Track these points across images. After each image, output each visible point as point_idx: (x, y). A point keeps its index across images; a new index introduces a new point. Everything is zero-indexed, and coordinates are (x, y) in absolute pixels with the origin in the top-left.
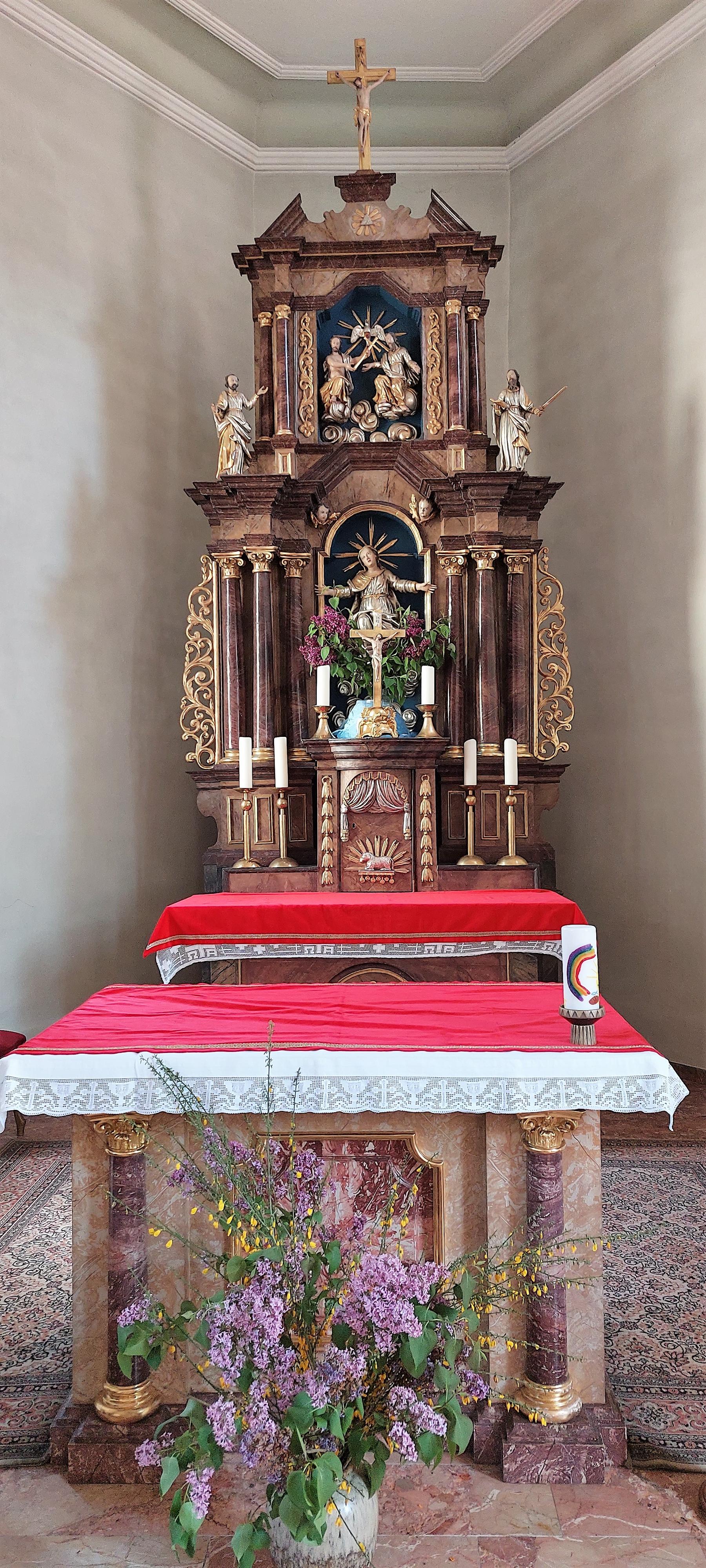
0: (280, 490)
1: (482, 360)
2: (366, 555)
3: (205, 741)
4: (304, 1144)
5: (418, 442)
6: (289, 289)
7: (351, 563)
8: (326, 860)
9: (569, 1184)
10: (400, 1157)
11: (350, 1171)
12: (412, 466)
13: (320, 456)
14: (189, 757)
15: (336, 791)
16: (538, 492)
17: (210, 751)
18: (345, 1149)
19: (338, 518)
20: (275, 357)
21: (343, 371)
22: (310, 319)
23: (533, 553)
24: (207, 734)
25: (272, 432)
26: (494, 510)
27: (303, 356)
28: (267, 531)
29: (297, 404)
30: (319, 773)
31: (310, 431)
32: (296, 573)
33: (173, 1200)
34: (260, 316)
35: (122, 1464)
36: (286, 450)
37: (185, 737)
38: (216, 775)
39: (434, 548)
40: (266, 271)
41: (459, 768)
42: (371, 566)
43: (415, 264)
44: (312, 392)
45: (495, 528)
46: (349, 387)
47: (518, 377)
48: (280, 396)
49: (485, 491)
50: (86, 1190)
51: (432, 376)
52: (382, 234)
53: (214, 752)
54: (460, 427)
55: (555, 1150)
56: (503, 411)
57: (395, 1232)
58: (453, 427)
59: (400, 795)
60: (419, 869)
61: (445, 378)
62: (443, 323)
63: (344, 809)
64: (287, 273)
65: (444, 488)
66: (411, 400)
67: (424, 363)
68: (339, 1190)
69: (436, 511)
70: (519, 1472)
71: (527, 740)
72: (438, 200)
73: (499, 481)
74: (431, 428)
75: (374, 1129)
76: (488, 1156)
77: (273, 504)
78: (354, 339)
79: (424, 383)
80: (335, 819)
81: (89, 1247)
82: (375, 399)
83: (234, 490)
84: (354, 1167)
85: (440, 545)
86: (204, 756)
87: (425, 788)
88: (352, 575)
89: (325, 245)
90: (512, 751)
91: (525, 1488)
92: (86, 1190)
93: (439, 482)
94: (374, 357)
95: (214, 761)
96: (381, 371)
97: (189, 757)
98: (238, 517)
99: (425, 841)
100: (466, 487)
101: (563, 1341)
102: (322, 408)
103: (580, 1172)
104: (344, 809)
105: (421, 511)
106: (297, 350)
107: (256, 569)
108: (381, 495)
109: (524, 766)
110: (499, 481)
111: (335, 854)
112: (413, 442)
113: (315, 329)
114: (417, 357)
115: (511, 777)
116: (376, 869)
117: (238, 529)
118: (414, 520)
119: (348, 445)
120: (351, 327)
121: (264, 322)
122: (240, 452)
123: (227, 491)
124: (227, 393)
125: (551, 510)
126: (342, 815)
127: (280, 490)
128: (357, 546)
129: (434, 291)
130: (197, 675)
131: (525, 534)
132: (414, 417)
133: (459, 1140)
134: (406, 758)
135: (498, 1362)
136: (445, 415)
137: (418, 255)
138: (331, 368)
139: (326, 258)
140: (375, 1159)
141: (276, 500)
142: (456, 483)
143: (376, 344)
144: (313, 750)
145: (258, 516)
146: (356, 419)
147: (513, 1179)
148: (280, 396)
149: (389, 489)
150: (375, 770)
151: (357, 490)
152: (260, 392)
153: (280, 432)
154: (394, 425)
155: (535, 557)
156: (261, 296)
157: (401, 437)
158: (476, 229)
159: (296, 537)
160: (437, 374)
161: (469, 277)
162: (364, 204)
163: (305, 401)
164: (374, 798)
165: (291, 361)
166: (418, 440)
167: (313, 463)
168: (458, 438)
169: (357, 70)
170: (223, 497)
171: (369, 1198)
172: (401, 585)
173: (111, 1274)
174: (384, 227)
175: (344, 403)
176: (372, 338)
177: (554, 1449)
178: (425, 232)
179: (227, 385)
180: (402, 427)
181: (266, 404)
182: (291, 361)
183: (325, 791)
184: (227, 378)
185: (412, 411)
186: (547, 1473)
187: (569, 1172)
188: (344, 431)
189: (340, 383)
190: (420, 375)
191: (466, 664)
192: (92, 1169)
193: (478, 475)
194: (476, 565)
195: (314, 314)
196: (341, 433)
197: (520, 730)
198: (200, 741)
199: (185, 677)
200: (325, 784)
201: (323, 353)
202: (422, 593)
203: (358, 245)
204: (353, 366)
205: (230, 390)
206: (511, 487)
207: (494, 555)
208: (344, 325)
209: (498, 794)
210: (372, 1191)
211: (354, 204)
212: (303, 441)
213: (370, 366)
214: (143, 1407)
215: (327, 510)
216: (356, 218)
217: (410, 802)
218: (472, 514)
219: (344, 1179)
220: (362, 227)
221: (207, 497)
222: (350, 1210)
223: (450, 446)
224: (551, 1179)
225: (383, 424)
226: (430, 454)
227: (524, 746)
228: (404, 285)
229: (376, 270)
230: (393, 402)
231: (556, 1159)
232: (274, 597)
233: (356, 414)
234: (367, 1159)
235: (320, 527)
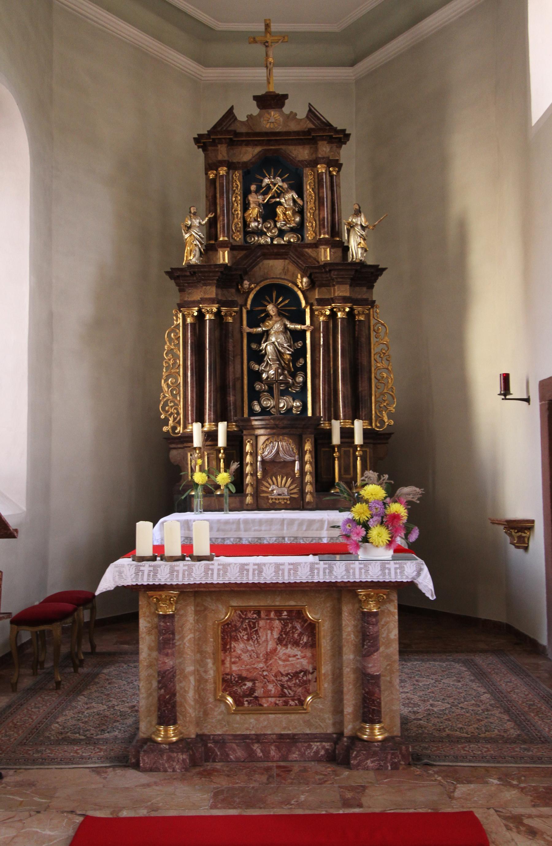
0: (221, 272)
1: (339, 197)
2: (271, 309)
3: (175, 419)
4: (252, 612)
5: (302, 244)
6: (226, 158)
7: (262, 313)
8: (249, 490)
9: (382, 628)
10: (299, 618)
11: (275, 625)
12: (298, 257)
13: (244, 252)
14: (165, 429)
15: (255, 448)
16: (372, 273)
17: (177, 425)
18: (272, 615)
19: (255, 287)
20: (218, 195)
21: (257, 203)
22: (237, 175)
23: (370, 309)
24: (176, 415)
25: (216, 238)
26: (346, 284)
27: (234, 195)
28: (213, 296)
29: (231, 222)
30: (245, 437)
31: (238, 237)
32: (230, 320)
33: (189, 637)
34: (209, 173)
35: (166, 762)
36: (224, 249)
37: (163, 417)
38: (182, 440)
39: (311, 305)
40: (213, 148)
41: (329, 434)
42: (275, 315)
43: (299, 144)
44: (239, 216)
45: (347, 294)
46: (261, 212)
47: (360, 208)
48: (221, 218)
49: (342, 273)
50: (146, 633)
51: (310, 206)
52: (280, 127)
53: (180, 426)
54: (327, 236)
55: (375, 610)
56: (351, 227)
57: (297, 655)
58: (322, 236)
59: (293, 450)
60: (304, 495)
61: (317, 208)
62: (316, 177)
63: (259, 458)
64: (225, 149)
65: (317, 271)
66: (298, 219)
67: (305, 199)
68: (269, 635)
69: (312, 284)
70: (358, 764)
71: (369, 418)
72: (313, 109)
73: (350, 268)
74: (309, 236)
75: (287, 604)
76: (343, 615)
77: (217, 280)
78: (264, 184)
79: (305, 211)
80: (254, 465)
81: (148, 661)
82: (277, 219)
83: (195, 273)
84: (277, 623)
85: (315, 303)
86: (174, 428)
87: (308, 447)
88: (263, 320)
89: (248, 134)
90: (358, 426)
91: (361, 772)
92: (146, 633)
93: (315, 268)
94: (276, 195)
95: (180, 431)
96: (280, 204)
97: (165, 429)
98: (196, 287)
99: (308, 478)
100: (330, 271)
101: (380, 703)
102: (246, 224)
103: (387, 623)
104: (259, 458)
105: (304, 284)
106: (231, 192)
107: (207, 317)
108: (280, 274)
109: (367, 433)
110: (350, 268)
111: (255, 486)
112: (299, 244)
113: (241, 180)
114: (301, 195)
115: (358, 439)
116: (279, 495)
117: (197, 295)
118: (300, 289)
119: (260, 246)
120: (262, 178)
121: (211, 176)
122: (197, 250)
123: (190, 273)
124: (190, 216)
125: (380, 285)
126: (258, 463)
127: (221, 272)
128: (266, 303)
129: (311, 159)
130: (170, 380)
131: (365, 297)
132: (299, 229)
133: (329, 609)
134: (296, 428)
135: (348, 716)
136: (317, 229)
137: (301, 139)
138: (251, 202)
139: (248, 141)
140: (287, 619)
141: (219, 277)
142: (324, 268)
143: (277, 188)
144: (241, 424)
145: (208, 287)
146: (265, 230)
147: (356, 626)
148: (221, 218)
149: (285, 271)
150: (279, 435)
151: (266, 271)
152: (210, 216)
153: (221, 239)
154: (288, 234)
155: (371, 310)
156: (210, 162)
157: (292, 240)
158: (335, 126)
159: (230, 299)
160: (313, 205)
161: (330, 151)
162: (270, 111)
163: (236, 220)
164: (277, 452)
165: (228, 198)
166: (302, 243)
167: (240, 256)
168: (325, 242)
169: (266, 36)
170: (187, 276)
171: (284, 639)
172: (291, 326)
173: (159, 673)
174: (281, 123)
175: (258, 222)
176: (275, 185)
177: (375, 754)
178: (305, 126)
179: (190, 212)
180: (292, 235)
181: (212, 224)
182: (228, 198)
183: (248, 448)
184: (190, 209)
185: (298, 226)
186: (372, 765)
187: (382, 623)
188: (258, 238)
189: (256, 210)
190: (303, 206)
191: (332, 372)
192: (149, 622)
193: (337, 264)
194: (337, 315)
195: (241, 172)
196: (256, 238)
197: (363, 413)
198: (171, 419)
199: (163, 381)
200: (248, 444)
201: (246, 192)
202: (304, 331)
203: (267, 134)
204: (264, 201)
205: (192, 215)
206: (356, 271)
207: (347, 310)
208: (259, 177)
209: (351, 451)
210: (286, 635)
211: (264, 111)
212: (234, 243)
213: (273, 200)
214: (174, 737)
215: (248, 283)
216: (265, 118)
217: (299, 454)
218: (334, 286)
219: (272, 629)
220: (269, 124)
221: (178, 277)
222: (275, 644)
223: (321, 247)
224: (373, 624)
225: (282, 233)
226: (309, 251)
227: (367, 422)
228: (293, 156)
229: (277, 147)
230: (287, 221)
231: (376, 614)
232: (217, 334)
233: (266, 228)
234: (283, 619)
235: (244, 293)
